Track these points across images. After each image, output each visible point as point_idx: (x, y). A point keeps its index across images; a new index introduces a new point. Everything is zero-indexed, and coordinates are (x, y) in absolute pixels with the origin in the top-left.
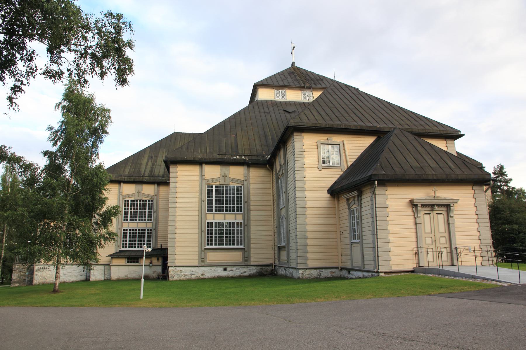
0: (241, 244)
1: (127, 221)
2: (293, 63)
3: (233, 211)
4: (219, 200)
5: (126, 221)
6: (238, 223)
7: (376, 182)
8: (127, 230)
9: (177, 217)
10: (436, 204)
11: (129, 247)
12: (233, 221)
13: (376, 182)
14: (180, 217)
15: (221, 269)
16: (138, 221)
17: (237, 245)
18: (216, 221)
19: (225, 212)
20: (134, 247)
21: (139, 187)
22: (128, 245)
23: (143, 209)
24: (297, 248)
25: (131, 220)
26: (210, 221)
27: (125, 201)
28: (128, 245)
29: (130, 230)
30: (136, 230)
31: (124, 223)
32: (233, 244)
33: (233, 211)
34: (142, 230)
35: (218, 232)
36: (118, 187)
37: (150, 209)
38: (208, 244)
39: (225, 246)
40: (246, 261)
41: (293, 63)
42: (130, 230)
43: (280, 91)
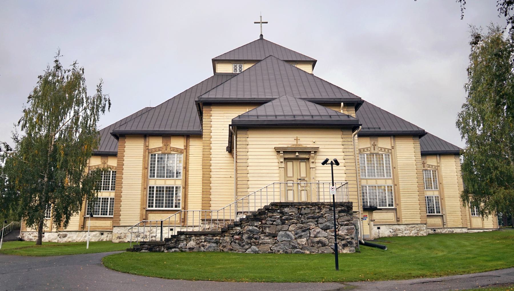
0: (112, 215)
1: (154, 178)
2: (261, 35)
3: (108, 190)
4: (107, 179)
5: (152, 178)
6: (111, 199)
7: (342, 104)
8: (153, 187)
9: (250, 157)
10: (298, 152)
11: (156, 207)
12: (107, 197)
13: (342, 104)
14: (253, 157)
15: (98, 233)
16: (165, 178)
17: (437, 213)
18: (157, 186)
19: (165, 178)
20: (151, 207)
21: (105, 159)
22: (154, 205)
23: (107, 179)
24: (335, 233)
25: (157, 177)
26: (152, 186)
27: (152, 155)
28: (154, 205)
29: (157, 187)
30: (163, 187)
31: (150, 180)
32: (107, 215)
33: (108, 190)
34: (105, 199)
35: (168, 199)
36: (143, 142)
37: (114, 177)
38: (149, 207)
39: (100, 216)
40: (398, 221)
41: (261, 35)
42: (157, 187)
43: (238, 65)
